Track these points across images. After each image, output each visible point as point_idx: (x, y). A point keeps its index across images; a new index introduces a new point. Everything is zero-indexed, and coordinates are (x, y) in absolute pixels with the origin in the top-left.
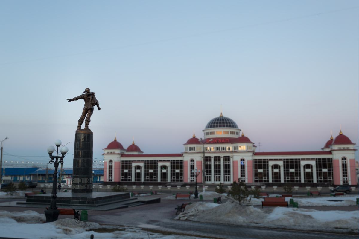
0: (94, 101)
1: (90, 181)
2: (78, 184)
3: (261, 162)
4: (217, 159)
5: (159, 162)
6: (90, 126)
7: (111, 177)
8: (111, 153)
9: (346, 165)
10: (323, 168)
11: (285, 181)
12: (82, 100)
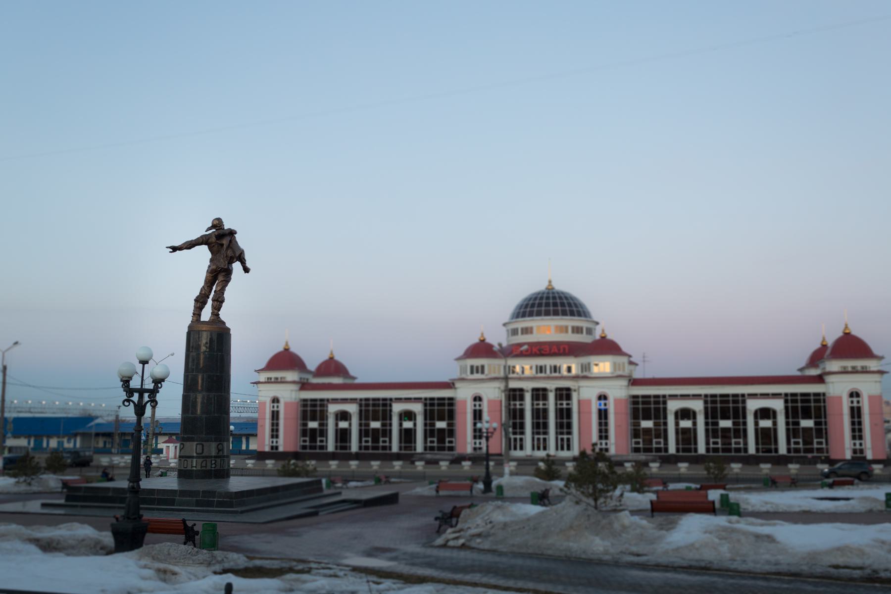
0: (234, 252)
1: (222, 450)
2: (192, 457)
3: (315, 406)
4: (540, 394)
5: (395, 402)
6: (223, 314)
8: (277, 381)
9: (859, 409)
12: (205, 248)
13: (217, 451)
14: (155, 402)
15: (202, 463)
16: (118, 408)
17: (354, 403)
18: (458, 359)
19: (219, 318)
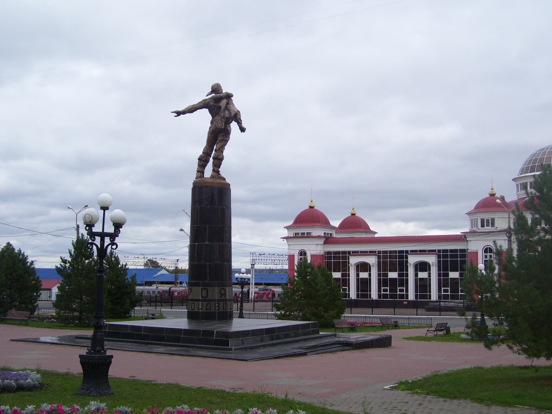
0: (230, 113)
1: (225, 294)
2: (198, 300)
5: (411, 254)
6: (223, 170)
8: (303, 236)
11: (379, 296)
12: (206, 111)
13: (220, 295)
14: (115, 245)
16: (176, 261)
17: (373, 255)
18: (469, 214)
19: (220, 174)
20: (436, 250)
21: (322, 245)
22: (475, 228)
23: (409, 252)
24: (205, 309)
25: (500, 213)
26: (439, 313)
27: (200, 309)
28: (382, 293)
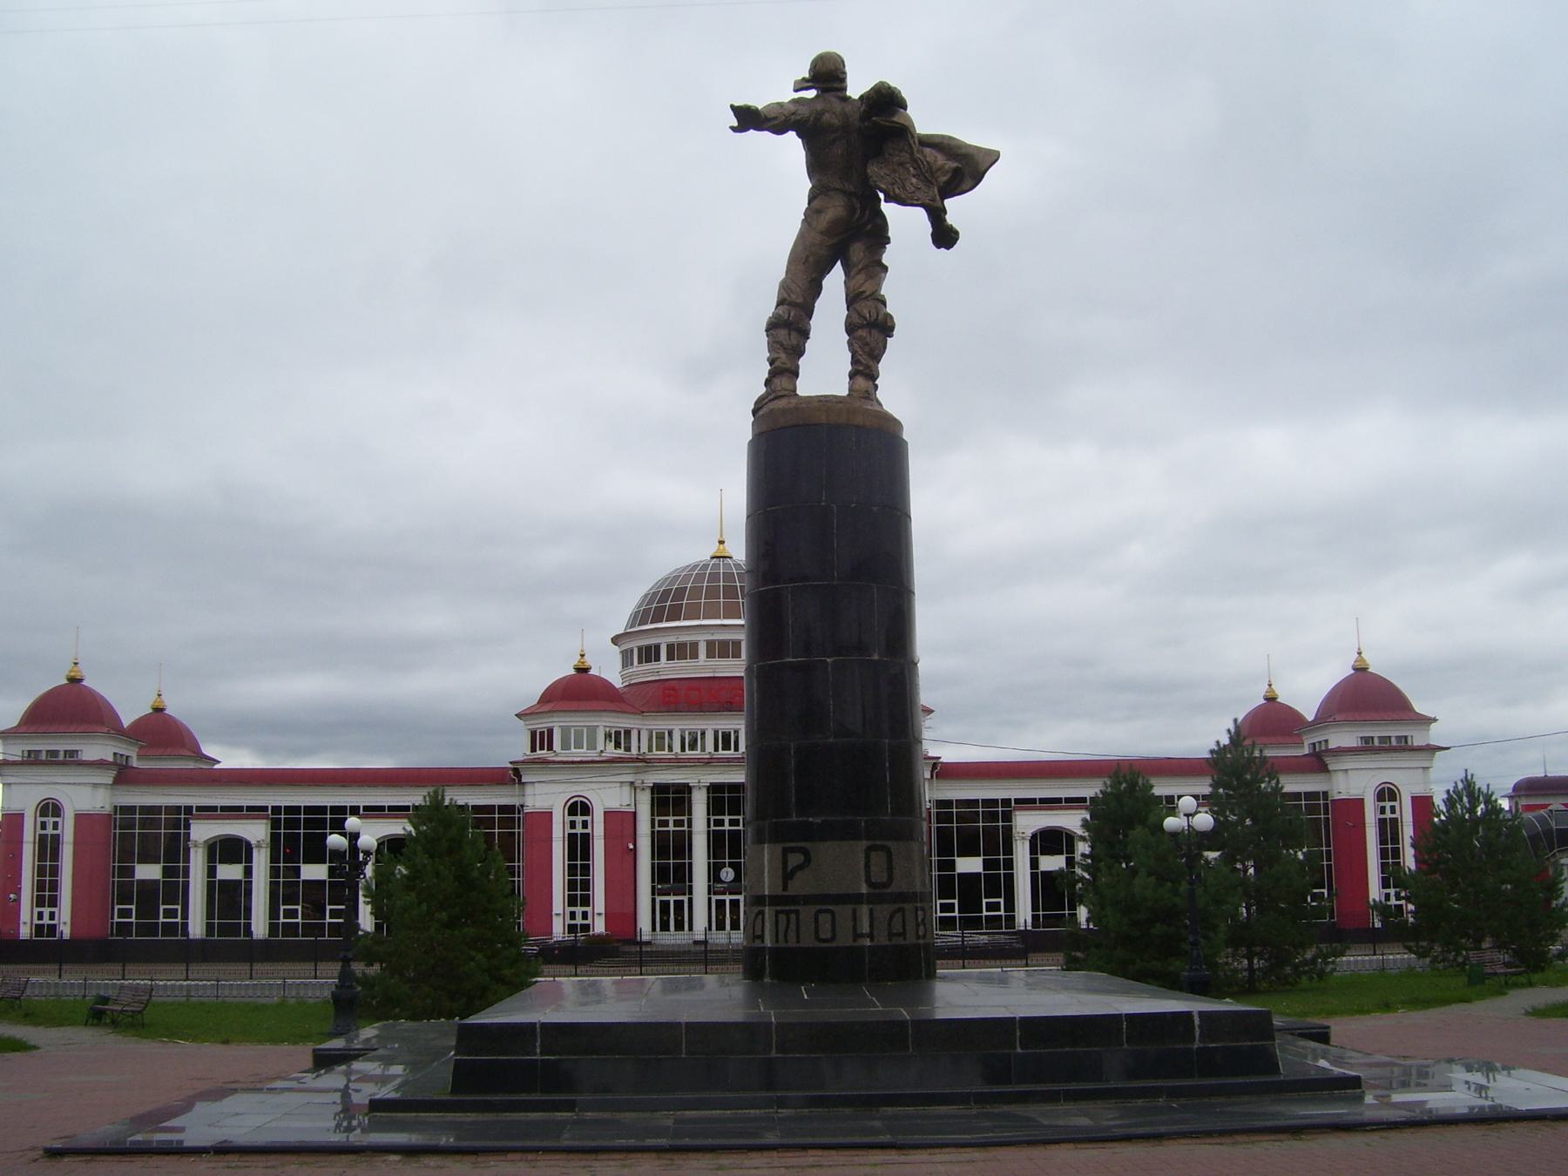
2: (857, 899)
5: (198, 818)
7: (46, 911)
8: (53, 761)
9: (1394, 821)
10: (307, 861)
11: (273, 928)
15: (891, 917)
20: (267, 807)
21: (109, 787)
22: (545, 751)
23: (194, 812)
24: (886, 933)
25: (585, 714)
26: (703, 967)
27: (862, 936)
28: (282, 920)
